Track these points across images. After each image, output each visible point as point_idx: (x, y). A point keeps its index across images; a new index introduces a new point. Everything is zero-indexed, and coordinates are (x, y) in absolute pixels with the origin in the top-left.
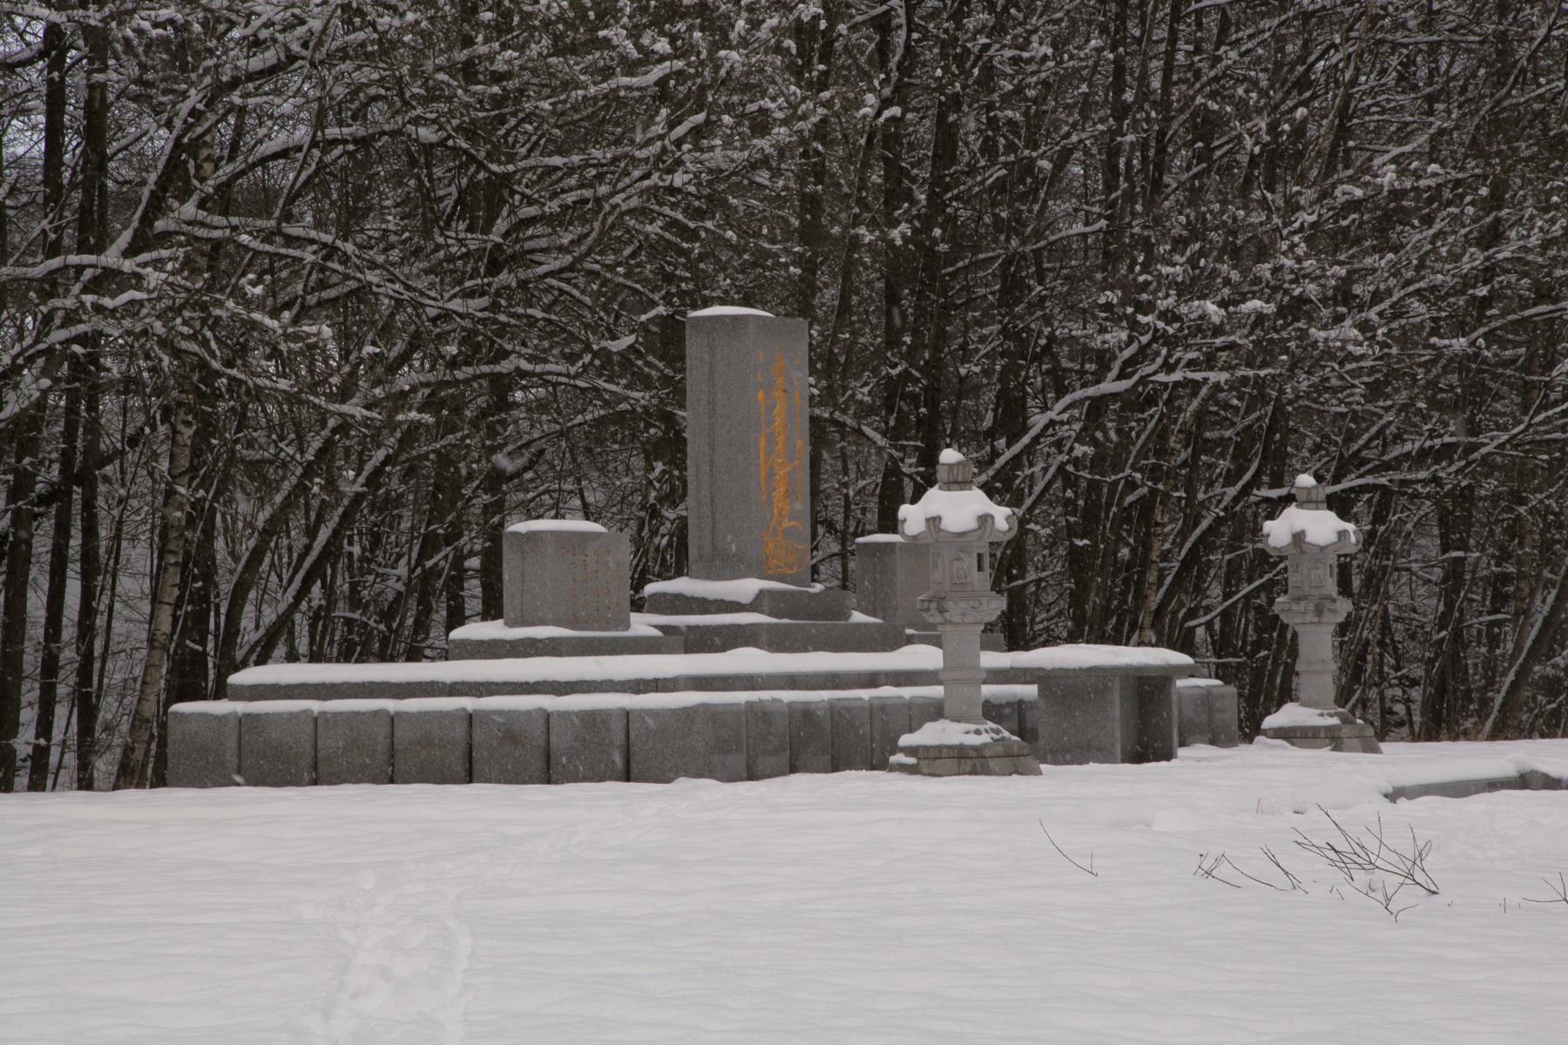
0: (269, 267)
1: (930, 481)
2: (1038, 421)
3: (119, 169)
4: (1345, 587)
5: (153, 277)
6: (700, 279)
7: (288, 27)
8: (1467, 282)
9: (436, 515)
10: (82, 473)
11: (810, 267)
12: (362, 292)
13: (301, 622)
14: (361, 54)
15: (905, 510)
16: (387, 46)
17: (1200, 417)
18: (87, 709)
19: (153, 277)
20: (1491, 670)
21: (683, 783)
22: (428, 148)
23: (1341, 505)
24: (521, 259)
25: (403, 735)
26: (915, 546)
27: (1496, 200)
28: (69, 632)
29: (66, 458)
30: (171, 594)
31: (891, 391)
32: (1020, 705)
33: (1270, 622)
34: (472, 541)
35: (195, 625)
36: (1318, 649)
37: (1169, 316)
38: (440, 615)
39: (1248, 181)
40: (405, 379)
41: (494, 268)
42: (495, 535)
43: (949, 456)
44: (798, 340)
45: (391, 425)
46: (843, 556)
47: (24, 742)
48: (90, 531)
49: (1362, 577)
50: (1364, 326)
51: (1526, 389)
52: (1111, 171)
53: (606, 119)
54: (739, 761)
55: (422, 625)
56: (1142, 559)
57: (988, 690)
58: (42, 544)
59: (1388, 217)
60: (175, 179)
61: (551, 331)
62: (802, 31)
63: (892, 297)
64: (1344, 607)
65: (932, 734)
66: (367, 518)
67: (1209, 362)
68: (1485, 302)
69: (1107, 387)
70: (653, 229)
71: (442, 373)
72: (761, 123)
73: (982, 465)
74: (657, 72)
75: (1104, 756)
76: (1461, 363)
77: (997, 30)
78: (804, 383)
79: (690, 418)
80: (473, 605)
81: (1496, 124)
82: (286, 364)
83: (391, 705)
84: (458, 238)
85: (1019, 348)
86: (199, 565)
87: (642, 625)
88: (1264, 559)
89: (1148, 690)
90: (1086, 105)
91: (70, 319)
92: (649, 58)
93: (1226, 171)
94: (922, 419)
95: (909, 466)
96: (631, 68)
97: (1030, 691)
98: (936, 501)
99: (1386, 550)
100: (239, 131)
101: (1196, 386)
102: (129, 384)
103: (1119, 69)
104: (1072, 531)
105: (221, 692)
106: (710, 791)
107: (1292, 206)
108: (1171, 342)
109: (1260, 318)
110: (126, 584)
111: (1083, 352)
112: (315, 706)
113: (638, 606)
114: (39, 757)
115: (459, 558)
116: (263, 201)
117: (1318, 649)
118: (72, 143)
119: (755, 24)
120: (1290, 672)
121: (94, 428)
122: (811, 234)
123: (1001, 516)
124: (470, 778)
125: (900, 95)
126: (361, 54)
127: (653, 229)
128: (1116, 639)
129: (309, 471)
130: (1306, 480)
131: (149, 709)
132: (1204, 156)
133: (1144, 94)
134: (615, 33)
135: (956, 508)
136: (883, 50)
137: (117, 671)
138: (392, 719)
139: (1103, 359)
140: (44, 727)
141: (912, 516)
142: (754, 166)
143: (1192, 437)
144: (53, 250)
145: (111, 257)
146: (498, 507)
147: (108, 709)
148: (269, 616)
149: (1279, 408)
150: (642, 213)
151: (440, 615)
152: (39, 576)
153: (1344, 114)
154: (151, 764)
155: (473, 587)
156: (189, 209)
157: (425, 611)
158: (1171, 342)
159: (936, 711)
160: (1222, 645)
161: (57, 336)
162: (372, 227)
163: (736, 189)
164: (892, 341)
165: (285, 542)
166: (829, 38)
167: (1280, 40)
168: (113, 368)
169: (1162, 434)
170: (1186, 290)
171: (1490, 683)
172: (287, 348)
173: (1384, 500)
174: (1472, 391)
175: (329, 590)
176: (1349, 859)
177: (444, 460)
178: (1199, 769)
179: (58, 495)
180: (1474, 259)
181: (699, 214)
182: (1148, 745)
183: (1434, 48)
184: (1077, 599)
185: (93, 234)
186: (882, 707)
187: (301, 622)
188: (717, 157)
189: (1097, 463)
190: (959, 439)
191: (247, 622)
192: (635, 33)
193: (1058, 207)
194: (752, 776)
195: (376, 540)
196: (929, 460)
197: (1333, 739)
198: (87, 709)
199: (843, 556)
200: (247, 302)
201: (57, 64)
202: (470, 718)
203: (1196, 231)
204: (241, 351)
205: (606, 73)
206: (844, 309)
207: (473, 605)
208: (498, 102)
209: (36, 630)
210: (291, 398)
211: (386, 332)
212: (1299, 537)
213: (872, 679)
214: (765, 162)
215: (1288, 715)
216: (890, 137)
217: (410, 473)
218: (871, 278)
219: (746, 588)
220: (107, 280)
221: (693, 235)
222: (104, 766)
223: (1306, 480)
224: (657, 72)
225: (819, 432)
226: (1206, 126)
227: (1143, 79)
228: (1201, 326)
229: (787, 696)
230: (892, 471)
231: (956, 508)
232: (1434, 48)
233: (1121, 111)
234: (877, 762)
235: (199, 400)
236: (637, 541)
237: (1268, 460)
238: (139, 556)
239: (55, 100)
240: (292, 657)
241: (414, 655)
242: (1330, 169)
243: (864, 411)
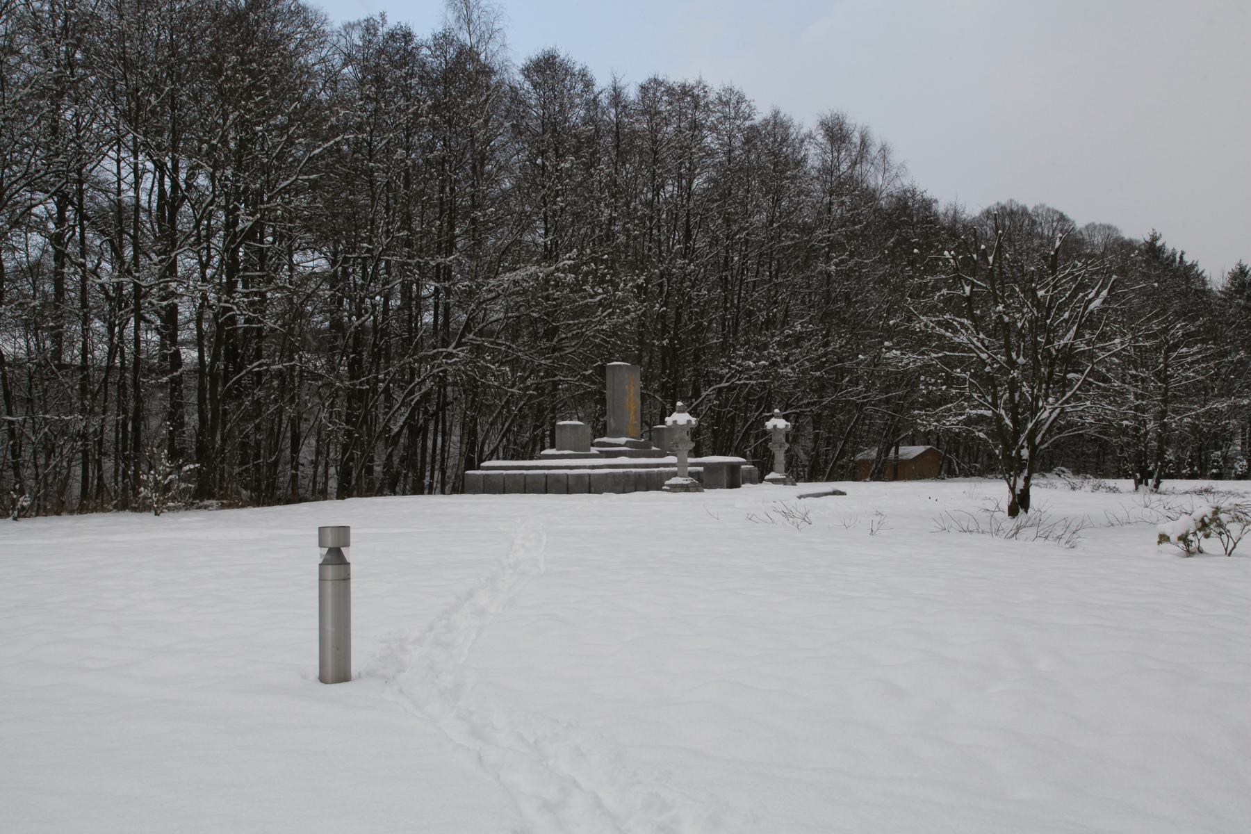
0: (492, 351)
1: (674, 410)
2: (704, 394)
3: (453, 325)
4: (787, 441)
5: (461, 355)
6: (611, 355)
7: (499, 286)
8: (820, 357)
9: (537, 420)
10: (443, 405)
11: (640, 351)
12: (518, 359)
13: (501, 450)
14: (517, 293)
15: (667, 419)
16: (525, 291)
17: (748, 393)
18: (443, 473)
19: (461, 355)
20: (826, 462)
21: (605, 494)
22: (536, 319)
23: (786, 418)
24: (562, 349)
25: (528, 481)
26: (670, 429)
27: (827, 335)
28: (438, 451)
29: (438, 404)
30: (465, 441)
31: (663, 385)
32: (698, 473)
33: (767, 450)
34: (547, 426)
35: (471, 449)
36: (780, 457)
37: (740, 365)
38: (538, 447)
39: (761, 329)
40: (529, 382)
41: (553, 352)
42: (554, 425)
43: (679, 404)
44: (639, 371)
45: (525, 395)
46: (650, 431)
47: (427, 481)
48: (444, 424)
49: (792, 437)
50: (793, 369)
51: (836, 386)
52: (723, 325)
53: (587, 311)
54: (620, 488)
55: (533, 450)
56: (732, 432)
57: (690, 469)
58: (431, 427)
59: (798, 339)
60: (467, 328)
61: (569, 369)
62: (639, 287)
63: (663, 360)
64: (787, 446)
65: (674, 481)
66: (519, 420)
67: (751, 378)
68: (825, 362)
69: (723, 385)
70: (597, 341)
71: (539, 380)
72: (627, 312)
73: (689, 406)
74: (598, 298)
75: (722, 487)
76: (818, 379)
77: (692, 287)
78: (640, 384)
79: (608, 392)
80: (547, 445)
81: (826, 315)
82: (497, 377)
83: (525, 472)
84: (544, 343)
85: (697, 373)
86: (473, 433)
87: (594, 450)
88: (765, 433)
89: (734, 468)
90: (717, 308)
91: (439, 366)
92: (597, 294)
93: (755, 326)
94: (670, 396)
95: (668, 406)
96: (592, 297)
97: (701, 469)
98: (675, 416)
99: (798, 430)
100: (485, 315)
101: (747, 385)
102: (455, 384)
103: (726, 298)
104: (713, 425)
105: (479, 468)
106: (612, 496)
107: (773, 336)
108: (741, 372)
109: (764, 366)
110: (454, 438)
111: (716, 375)
112: (504, 472)
113: (593, 445)
114: (431, 485)
115: (544, 431)
116: (491, 333)
117: (780, 457)
118: (441, 318)
119: (626, 285)
120: (772, 463)
121: (445, 396)
122: (641, 342)
123: (693, 420)
124: (546, 492)
125: (665, 304)
126: (517, 293)
127: (597, 341)
128: (724, 454)
129: (503, 407)
130: (777, 411)
131: (460, 472)
132: (749, 321)
133: (733, 304)
134: (587, 288)
135: (681, 418)
136: (661, 292)
137: (451, 462)
138: (525, 476)
139: (722, 377)
140: (432, 477)
141: (669, 420)
142: (625, 323)
143: (746, 398)
144: (435, 348)
145: (450, 349)
146: (554, 417)
147: (449, 472)
148: (492, 447)
149: (770, 392)
150: (594, 336)
151: (538, 447)
152: (431, 436)
153: (786, 311)
154: (460, 487)
155: (548, 440)
156: (471, 336)
157: (535, 445)
158: (741, 372)
159: (675, 474)
160: (754, 456)
161: (435, 371)
162: (520, 341)
163: (621, 330)
164: (664, 372)
165: (289, 411)
166: (646, 289)
167: (769, 290)
168: (450, 379)
169: (738, 397)
170: (744, 358)
171: (826, 466)
172: (497, 374)
173: (798, 416)
174: (821, 388)
175: (508, 440)
176: (787, 515)
177: (540, 404)
178: (747, 488)
179: (435, 414)
180: (821, 351)
181: (610, 337)
182: (734, 484)
183: (810, 294)
184: (715, 443)
185: (446, 344)
186: (660, 474)
187: (501, 450)
188: (615, 319)
189: (720, 406)
190: (682, 400)
191: (486, 449)
192: (593, 287)
193: (709, 335)
194: (624, 492)
195: (521, 426)
196: (674, 405)
197: (783, 482)
198: (443, 473)
199: (650, 431)
200: (487, 361)
201: (437, 297)
202: (546, 476)
203: (747, 342)
204: (484, 376)
205: (585, 298)
206: (650, 362)
207: (547, 445)
208: (555, 306)
209: (430, 451)
210: (498, 387)
211: (524, 369)
212: (775, 426)
213: (658, 466)
214: (628, 322)
215: (772, 475)
216: (663, 316)
217: (530, 408)
218: (658, 354)
219: (623, 440)
220: (450, 355)
221: (608, 343)
222: (448, 487)
223: (777, 411)
224: (598, 298)
225: (643, 397)
226: (750, 314)
227: (732, 301)
228: (749, 368)
229: (634, 470)
230: (663, 408)
231: (681, 418)
232: (810, 294)
233: (726, 309)
234: (659, 489)
235: (472, 388)
236: (593, 427)
237: (767, 406)
238: (457, 431)
239: (436, 307)
240: (498, 459)
241: (531, 458)
242: (783, 326)
243: (656, 391)
